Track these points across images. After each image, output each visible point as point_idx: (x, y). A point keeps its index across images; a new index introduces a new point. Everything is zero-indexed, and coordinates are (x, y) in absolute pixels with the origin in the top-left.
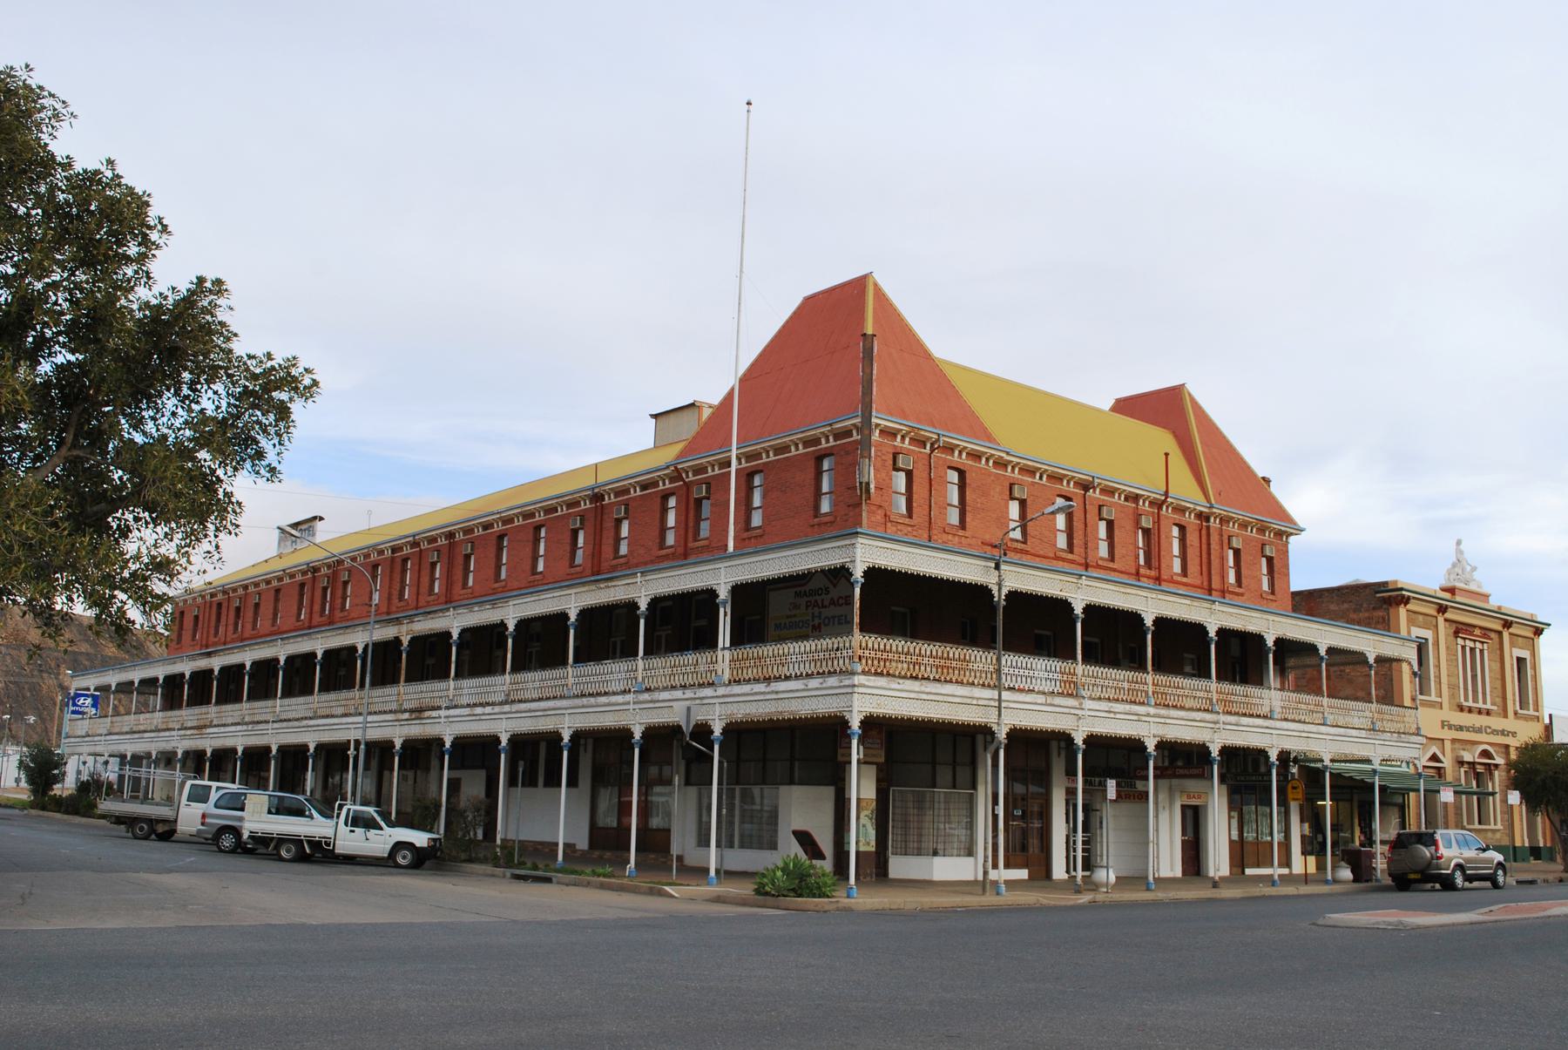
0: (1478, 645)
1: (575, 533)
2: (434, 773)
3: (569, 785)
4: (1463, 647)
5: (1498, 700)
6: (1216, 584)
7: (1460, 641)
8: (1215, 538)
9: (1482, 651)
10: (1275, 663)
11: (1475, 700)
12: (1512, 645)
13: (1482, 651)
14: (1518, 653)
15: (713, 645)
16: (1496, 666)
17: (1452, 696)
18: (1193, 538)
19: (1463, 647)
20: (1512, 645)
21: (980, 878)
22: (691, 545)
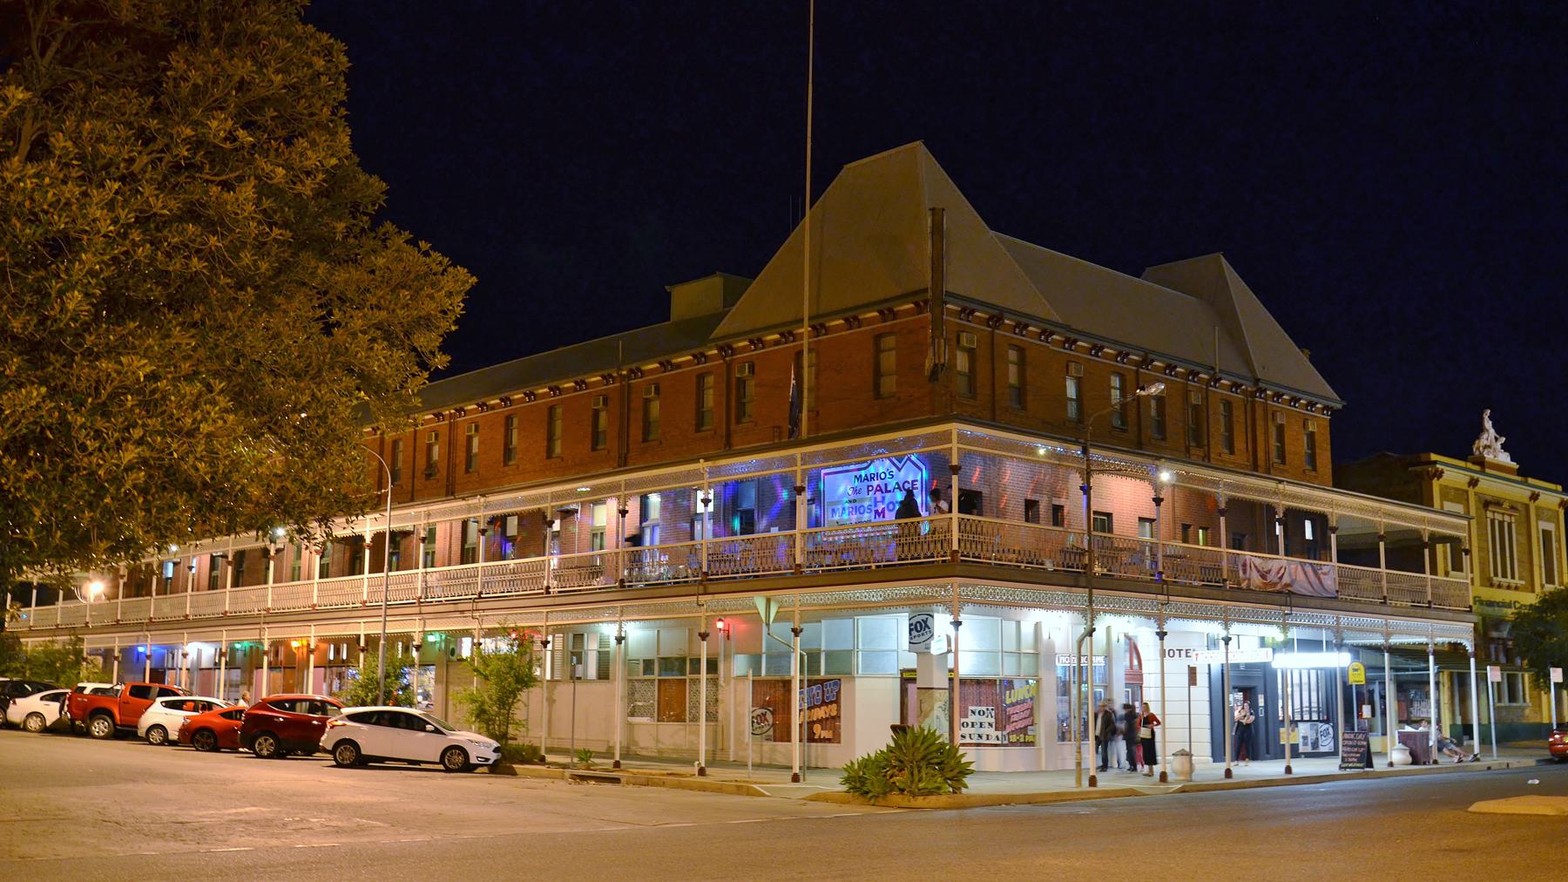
0: (1507, 518)
1: (596, 414)
2: (74, 799)
3: (699, 660)
4: (1493, 521)
5: (1526, 574)
6: (1261, 462)
7: (1489, 515)
8: (1259, 413)
9: (1510, 525)
10: (766, 460)
11: (1505, 575)
12: (1539, 518)
13: (1510, 525)
14: (1544, 525)
15: (361, 572)
16: (1524, 540)
17: (1483, 571)
18: (1238, 414)
19: (1493, 521)
20: (1539, 518)
21: (1095, 480)
22: (733, 427)
